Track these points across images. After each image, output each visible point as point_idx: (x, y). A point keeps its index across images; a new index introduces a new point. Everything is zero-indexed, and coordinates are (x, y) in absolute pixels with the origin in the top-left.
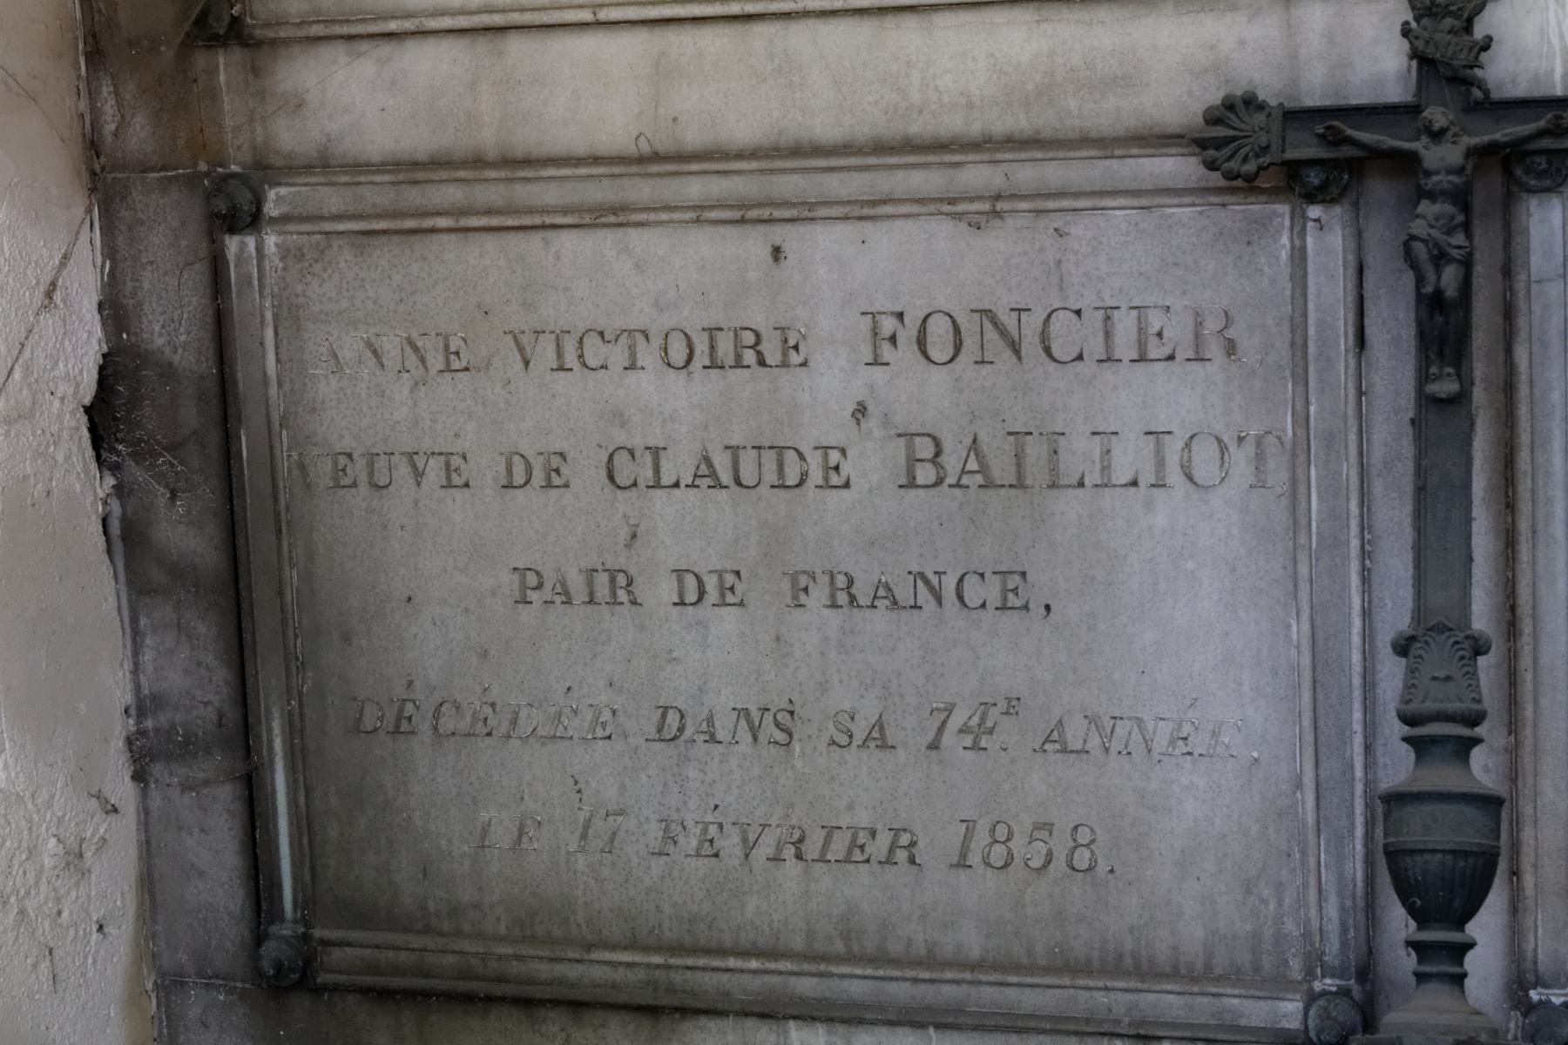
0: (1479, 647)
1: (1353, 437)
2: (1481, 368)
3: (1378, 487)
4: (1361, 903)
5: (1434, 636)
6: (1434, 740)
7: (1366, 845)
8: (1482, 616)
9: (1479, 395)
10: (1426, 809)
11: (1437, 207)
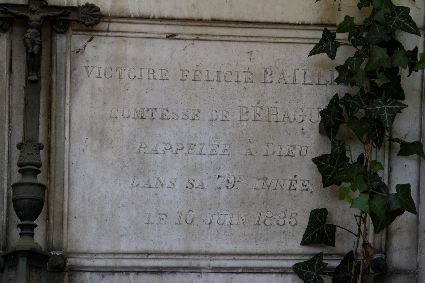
0: (40, 147)
1: (7, 97)
2: (44, 71)
3: (14, 111)
4: (5, 228)
5: (28, 143)
6: (28, 170)
7: (7, 212)
8: (41, 139)
9: (43, 81)
10: (25, 187)
11: (33, 30)
